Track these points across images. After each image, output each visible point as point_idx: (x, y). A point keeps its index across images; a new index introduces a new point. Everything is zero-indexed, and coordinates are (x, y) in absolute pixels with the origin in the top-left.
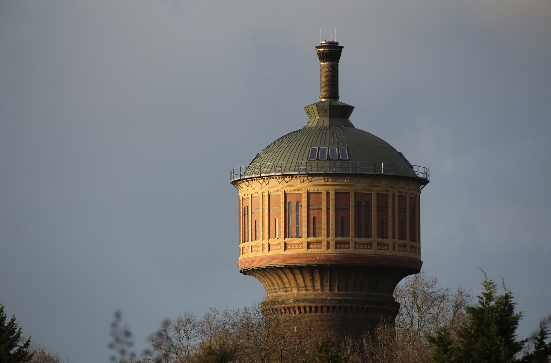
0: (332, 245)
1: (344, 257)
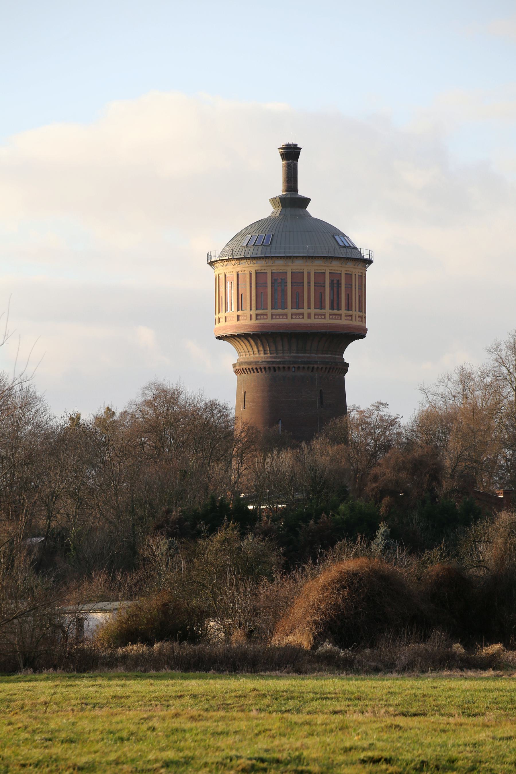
0: (254, 317)
1: (262, 326)
